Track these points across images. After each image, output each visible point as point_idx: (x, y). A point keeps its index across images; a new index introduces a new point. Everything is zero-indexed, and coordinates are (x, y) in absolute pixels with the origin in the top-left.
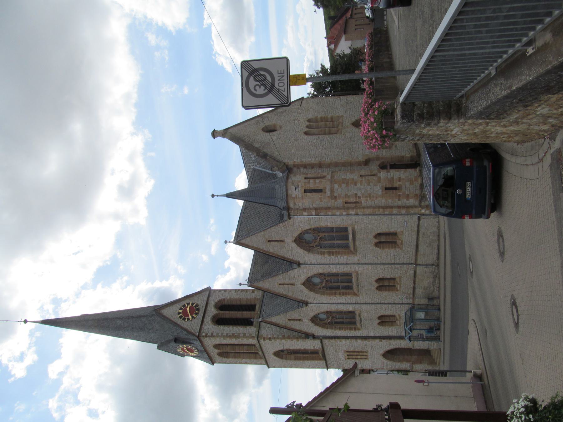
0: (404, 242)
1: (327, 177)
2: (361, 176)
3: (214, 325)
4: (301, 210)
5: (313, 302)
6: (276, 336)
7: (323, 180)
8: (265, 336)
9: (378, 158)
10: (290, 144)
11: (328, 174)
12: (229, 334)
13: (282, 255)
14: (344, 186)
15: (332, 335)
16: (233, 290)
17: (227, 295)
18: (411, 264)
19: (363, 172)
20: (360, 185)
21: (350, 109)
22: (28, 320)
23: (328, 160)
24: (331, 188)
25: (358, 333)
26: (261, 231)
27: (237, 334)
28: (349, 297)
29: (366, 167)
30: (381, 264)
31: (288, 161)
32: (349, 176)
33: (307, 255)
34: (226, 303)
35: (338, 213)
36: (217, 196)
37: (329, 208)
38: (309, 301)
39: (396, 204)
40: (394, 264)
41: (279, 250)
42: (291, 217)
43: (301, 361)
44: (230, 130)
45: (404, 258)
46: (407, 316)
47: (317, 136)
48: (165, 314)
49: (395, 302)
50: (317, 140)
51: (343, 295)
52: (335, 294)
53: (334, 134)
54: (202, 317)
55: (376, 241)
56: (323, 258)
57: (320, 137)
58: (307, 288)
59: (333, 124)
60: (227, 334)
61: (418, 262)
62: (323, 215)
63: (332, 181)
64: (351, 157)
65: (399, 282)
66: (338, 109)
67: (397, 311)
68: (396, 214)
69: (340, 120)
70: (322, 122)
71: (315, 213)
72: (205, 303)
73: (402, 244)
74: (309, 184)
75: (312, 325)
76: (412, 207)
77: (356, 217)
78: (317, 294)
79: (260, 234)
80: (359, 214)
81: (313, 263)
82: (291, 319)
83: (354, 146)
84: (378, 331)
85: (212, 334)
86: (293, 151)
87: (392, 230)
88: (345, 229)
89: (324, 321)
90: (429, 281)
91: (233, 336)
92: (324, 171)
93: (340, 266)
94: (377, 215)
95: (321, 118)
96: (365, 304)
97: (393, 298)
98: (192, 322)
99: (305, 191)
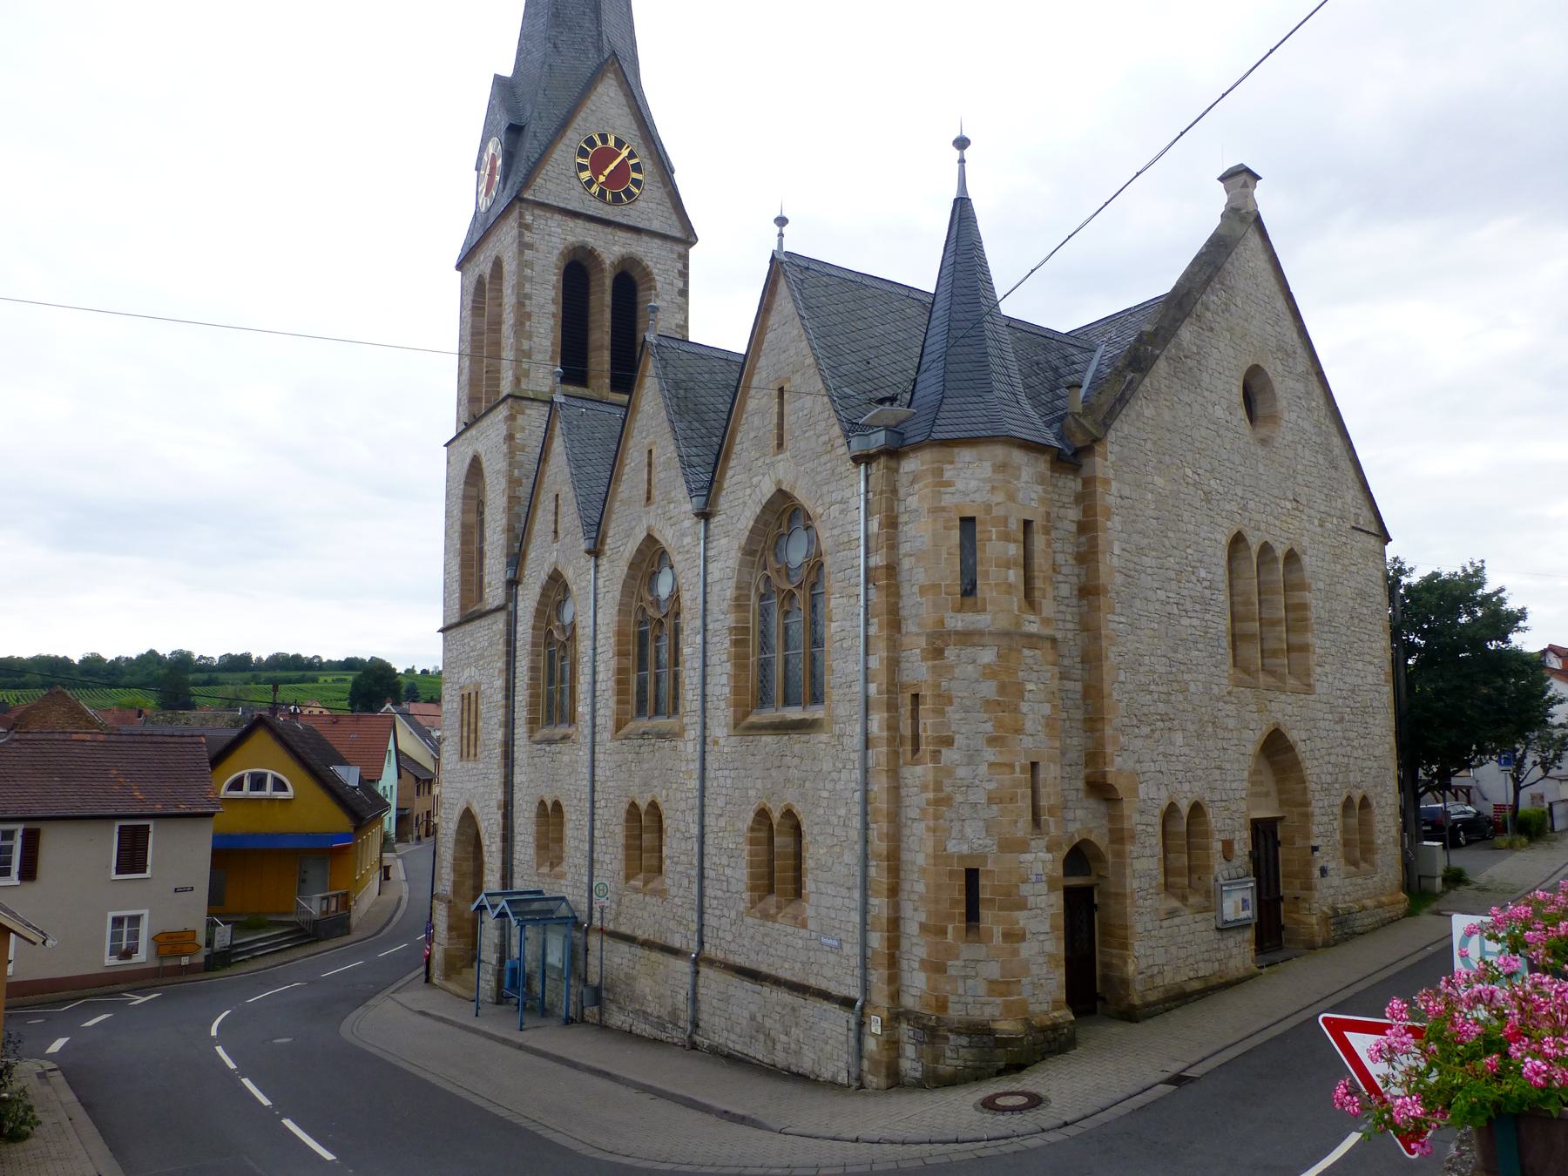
0: (770, 924)
1: (1032, 618)
2: (1034, 765)
3: (562, 253)
4: (890, 508)
5: (599, 575)
6: (518, 458)
7: (1017, 600)
8: (520, 420)
9: (1119, 836)
10: (1189, 472)
11: (1046, 622)
12: (527, 302)
13: (737, 448)
14: (989, 689)
15: (518, 644)
16: (686, 320)
17: (668, 298)
18: (701, 943)
19: (1050, 773)
20: (992, 759)
21: (1341, 720)
23: (1115, 626)
24: (981, 633)
25: (521, 731)
26: (813, 348)
27: (527, 328)
28: (612, 703)
29: (1081, 784)
30: (702, 826)
31: (1111, 458)
32: (1035, 711)
33: (735, 545)
34: (641, 295)
35: (875, 663)
36: (962, 161)
37: (895, 623)
38: (604, 561)
39: (907, 910)
40: (702, 876)
41: (752, 435)
42: (862, 467)
43: (458, 546)
44: (1254, 240)
45: (720, 917)
46: (557, 902)
47: (1224, 586)
48: (601, 89)
49: (597, 866)
50: (1206, 584)
51: (619, 682)
52: (621, 654)
53: (1234, 656)
54: (590, 213)
55: (776, 816)
56: (725, 605)
57: (1222, 598)
58: (639, 550)
59: (1275, 653)
60: (528, 297)
61: (704, 970)
62: (867, 600)
63: (1013, 640)
64: (1126, 720)
65: (651, 886)
66: (1338, 676)
67: (573, 870)
68: (865, 911)
69: (1292, 682)
70: (1286, 608)
71: (877, 568)
72: (640, 226)
73: (766, 916)
74: (999, 539)
75: (544, 577)
76: (894, 978)
77: (857, 741)
78: (620, 587)
79: (807, 351)
80: (870, 751)
81: (711, 567)
82: (560, 502)
83: (1178, 738)
84: (527, 798)
85: (530, 246)
86: (1159, 481)
87: (809, 885)
88: (816, 697)
89: (557, 615)
90: (650, 998)
91: (523, 316)
92: (1062, 608)
93: (699, 672)
94: (866, 827)
95: (1304, 607)
96: (593, 760)
97: (607, 857)
98: (575, 181)
99: (968, 523)
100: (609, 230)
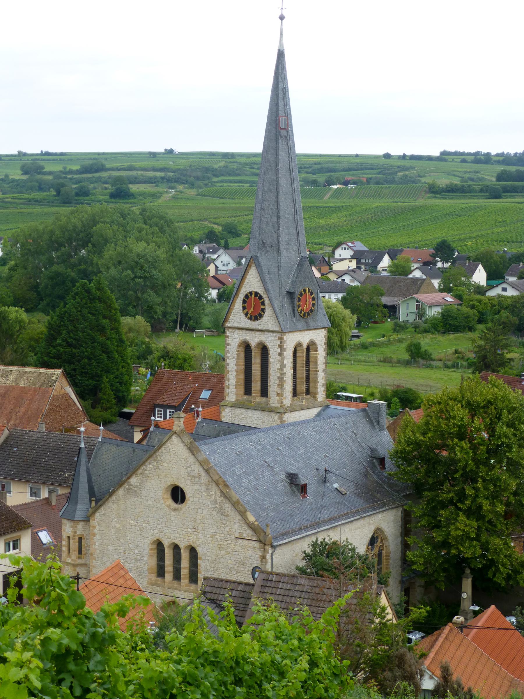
11: (72, 560)
17: (274, 357)
22: (283, 21)
100: (254, 332)
